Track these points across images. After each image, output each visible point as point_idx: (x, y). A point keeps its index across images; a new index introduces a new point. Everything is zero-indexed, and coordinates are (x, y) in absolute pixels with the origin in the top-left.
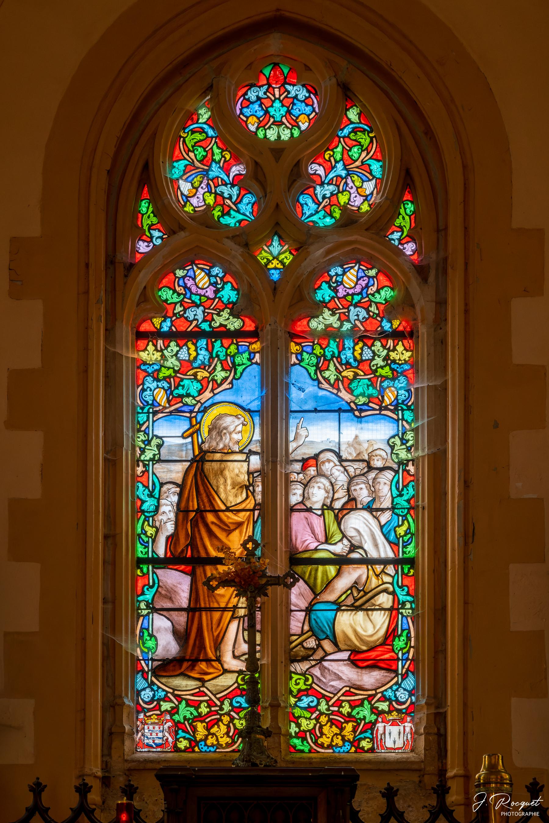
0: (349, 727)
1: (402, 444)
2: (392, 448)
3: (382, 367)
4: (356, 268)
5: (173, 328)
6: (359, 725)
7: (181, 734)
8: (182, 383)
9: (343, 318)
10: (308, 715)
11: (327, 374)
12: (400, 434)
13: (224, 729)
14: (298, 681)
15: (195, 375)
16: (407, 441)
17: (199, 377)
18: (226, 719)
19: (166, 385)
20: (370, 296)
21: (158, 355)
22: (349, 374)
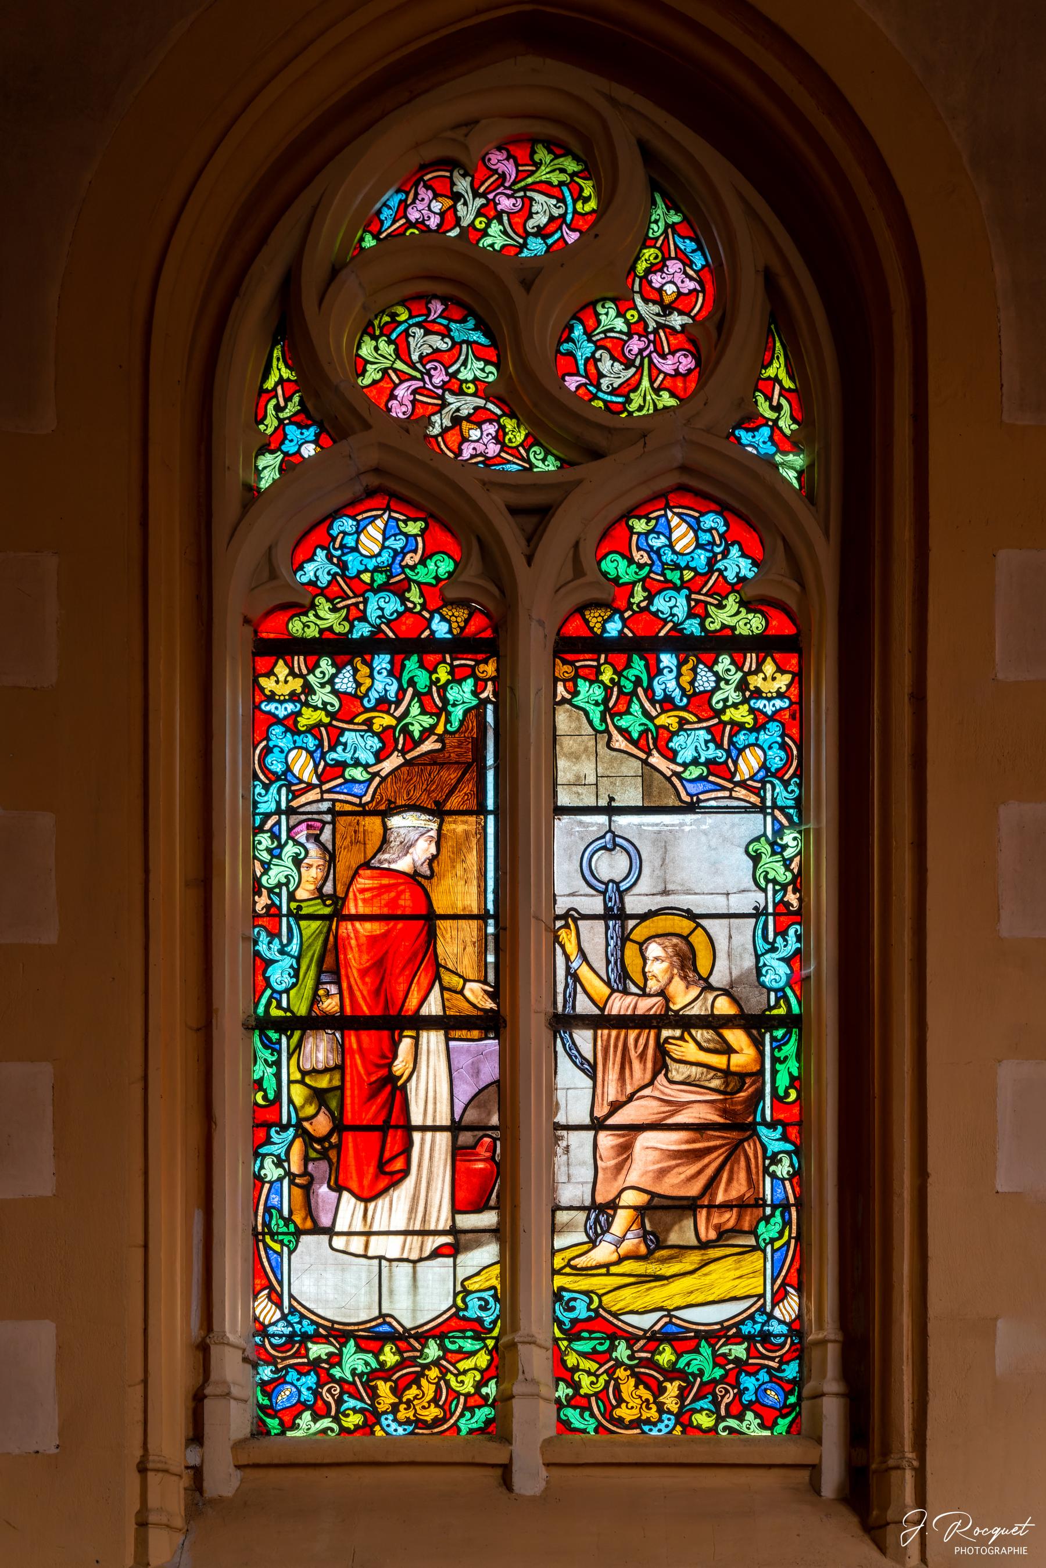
0: (672, 1389)
1: (774, 853)
2: (756, 859)
3: (735, 706)
4: (386, 517)
5: (626, 631)
6: (691, 1385)
7: (351, 1403)
8: (343, 740)
9: (354, 612)
10: (593, 1366)
11: (624, 722)
12: (769, 833)
13: (430, 1391)
14: (572, 1304)
15: (369, 722)
16: (784, 847)
17: (376, 728)
18: (434, 1373)
19: (311, 742)
20: (407, 570)
21: (296, 684)
22: (668, 720)
